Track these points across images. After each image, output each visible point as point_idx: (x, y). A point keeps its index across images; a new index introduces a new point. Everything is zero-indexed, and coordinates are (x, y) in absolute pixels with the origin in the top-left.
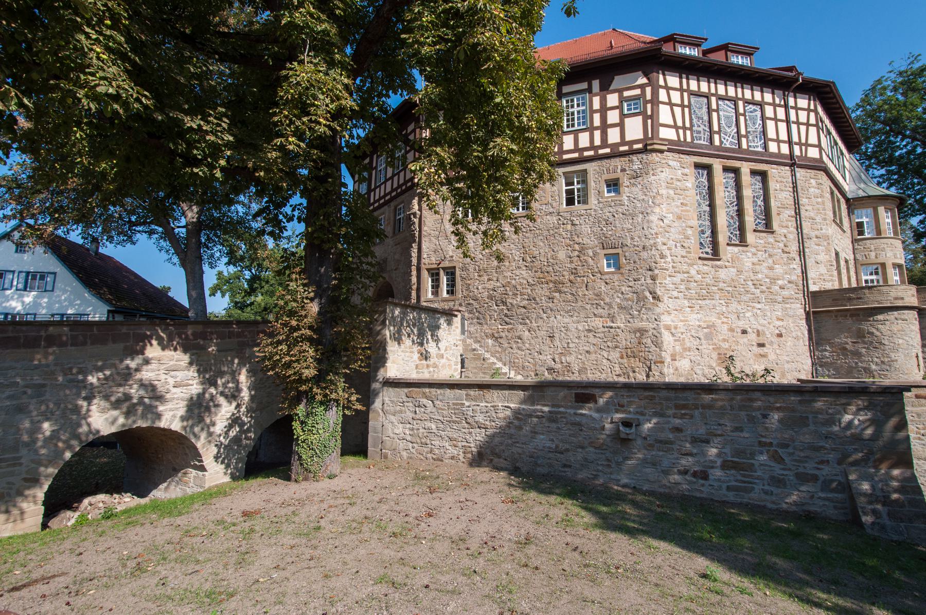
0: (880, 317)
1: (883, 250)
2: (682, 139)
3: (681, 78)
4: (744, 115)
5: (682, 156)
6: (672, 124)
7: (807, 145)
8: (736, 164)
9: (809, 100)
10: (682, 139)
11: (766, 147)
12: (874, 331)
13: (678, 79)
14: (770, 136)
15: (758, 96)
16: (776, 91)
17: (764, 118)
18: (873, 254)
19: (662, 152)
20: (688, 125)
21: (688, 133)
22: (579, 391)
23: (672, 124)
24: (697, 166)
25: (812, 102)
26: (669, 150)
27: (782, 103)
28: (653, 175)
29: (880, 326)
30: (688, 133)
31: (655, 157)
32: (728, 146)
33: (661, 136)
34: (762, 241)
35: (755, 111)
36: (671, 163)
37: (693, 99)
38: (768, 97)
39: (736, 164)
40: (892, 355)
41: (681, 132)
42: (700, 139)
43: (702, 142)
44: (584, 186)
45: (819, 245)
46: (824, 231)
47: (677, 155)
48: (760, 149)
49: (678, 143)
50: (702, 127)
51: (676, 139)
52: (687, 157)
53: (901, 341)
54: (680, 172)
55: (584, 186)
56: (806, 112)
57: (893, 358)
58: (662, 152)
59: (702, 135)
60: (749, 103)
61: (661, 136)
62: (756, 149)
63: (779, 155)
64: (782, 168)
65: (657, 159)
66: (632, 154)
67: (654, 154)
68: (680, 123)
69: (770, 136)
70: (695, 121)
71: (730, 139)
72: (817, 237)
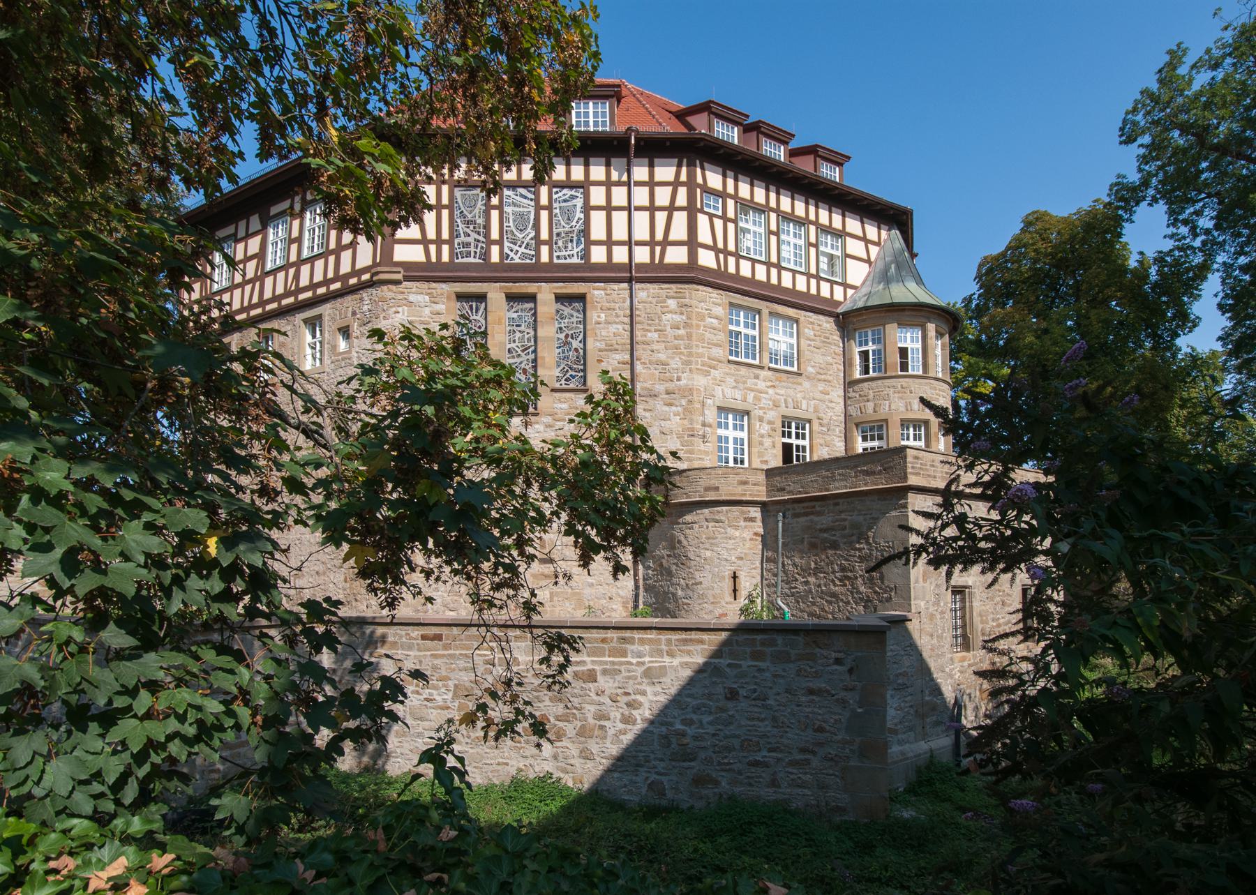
0: (688, 518)
1: (887, 398)
2: (434, 259)
3: (725, 176)
4: (549, 208)
5: (434, 285)
6: (711, 243)
7: (666, 243)
8: (530, 288)
9: (679, 166)
10: (434, 259)
11: (586, 255)
12: (682, 538)
13: (720, 177)
14: (594, 237)
15: (578, 173)
16: (613, 160)
17: (587, 208)
18: (870, 405)
19: (397, 282)
20: (445, 235)
21: (445, 248)
22: (669, 621)
23: (711, 243)
24: (460, 297)
25: (684, 169)
26: (407, 279)
27: (625, 178)
28: (385, 318)
29: (688, 531)
30: (445, 248)
31: (385, 291)
32: (517, 260)
33: (396, 258)
34: (564, 406)
35: (573, 197)
36: (412, 298)
37: (458, 193)
38: (598, 172)
39: (530, 288)
40: (697, 575)
41: (433, 248)
42: (468, 254)
43: (471, 260)
44: (881, 347)
45: (671, 405)
46: (683, 382)
47: (425, 285)
48: (575, 260)
49: (428, 265)
50: (474, 235)
51: (424, 260)
52: (443, 286)
53: (708, 554)
54: (427, 311)
55: (881, 347)
56: (646, 189)
57: (699, 580)
58: (397, 282)
59: (472, 249)
60: (563, 187)
61: (396, 258)
62: (568, 261)
63: (610, 265)
64: (615, 286)
65: (390, 295)
66: (362, 288)
67: (385, 288)
68: (720, 245)
69: (594, 237)
70: (462, 227)
71: (522, 250)
72: (668, 393)
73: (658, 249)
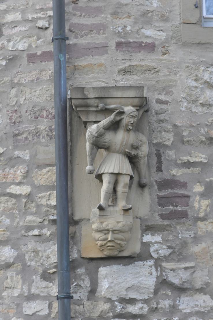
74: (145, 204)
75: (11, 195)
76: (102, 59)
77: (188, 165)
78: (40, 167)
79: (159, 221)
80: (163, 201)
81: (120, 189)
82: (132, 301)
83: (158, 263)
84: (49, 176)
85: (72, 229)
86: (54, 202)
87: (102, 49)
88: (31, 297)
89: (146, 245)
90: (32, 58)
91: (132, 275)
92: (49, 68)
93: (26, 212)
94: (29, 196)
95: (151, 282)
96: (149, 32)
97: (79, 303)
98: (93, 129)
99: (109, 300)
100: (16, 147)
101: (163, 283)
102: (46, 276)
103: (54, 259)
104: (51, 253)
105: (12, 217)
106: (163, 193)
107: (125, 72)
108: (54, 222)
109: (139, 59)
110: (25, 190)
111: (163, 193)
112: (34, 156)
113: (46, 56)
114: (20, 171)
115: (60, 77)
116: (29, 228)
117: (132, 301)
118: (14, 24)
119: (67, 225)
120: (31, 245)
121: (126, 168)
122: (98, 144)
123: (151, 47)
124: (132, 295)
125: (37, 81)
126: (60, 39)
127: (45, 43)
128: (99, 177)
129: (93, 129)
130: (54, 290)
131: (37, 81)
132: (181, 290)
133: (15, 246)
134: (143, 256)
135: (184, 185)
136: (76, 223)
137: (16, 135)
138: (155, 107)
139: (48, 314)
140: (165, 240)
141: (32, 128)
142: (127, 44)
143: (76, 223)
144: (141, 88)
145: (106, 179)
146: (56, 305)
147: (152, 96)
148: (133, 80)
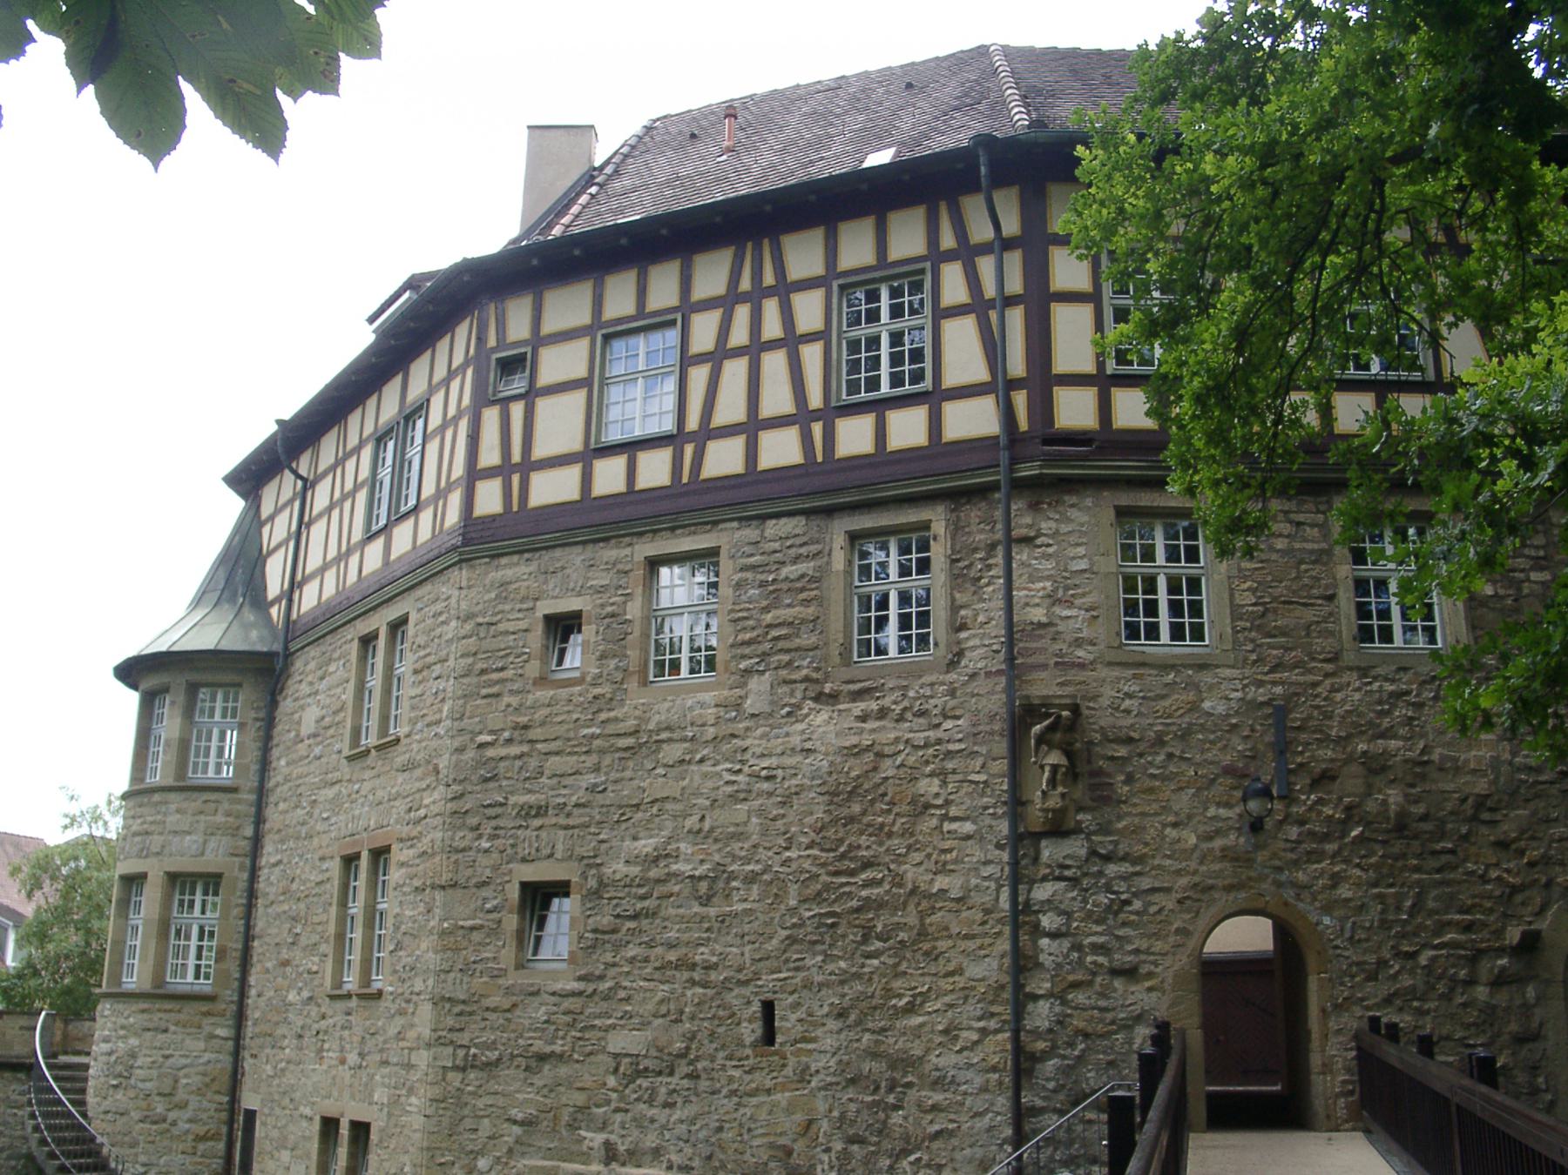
73: (817, 429)
74: (1079, 792)
75: (971, 782)
76: (1043, 675)
77: (1112, 758)
78: (994, 759)
79: (1090, 803)
80: (1093, 788)
81: (1059, 777)
82: (1068, 867)
83: (1088, 836)
84: (1001, 766)
85: (1020, 809)
86: (1005, 787)
87: (1044, 666)
88: (987, 863)
89: (1080, 822)
90: (988, 674)
91: (883, 713)
92: (1003, 681)
93: (983, 794)
94: (985, 782)
95: (1083, 852)
96: (1080, 653)
97: (1026, 867)
98: (1037, 728)
99: (1049, 866)
100: (975, 744)
101: (1093, 853)
102: (999, 846)
103: (1006, 831)
104: (1004, 827)
105: (973, 799)
106: (344, 1130)
107: (1061, 684)
108: (1005, 803)
109: (1072, 675)
110: (983, 777)
111: (344, 1130)
112: (989, 751)
113: (999, 672)
114: (979, 762)
115: (1010, 690)
116: (986, 808)
117: (1068, 867)
118: (974, 648)
119: (1016, 803)
120: (988, 821)
121: (1064, 761)
122: (1041, 740)
123: (1082, 666)
124: (1068, 862)
125: (992, 692)
126: (1011, 659)
127: (998, 664)
128: (1042, 767)
129: (1037, 728)
130: (1005, 856)
131: (992, 692)
132: (1107, 858)
133: (974, 822)
134: (1077, 831)
135: (1109, 775)
136: (1023, 804)
137: (975, 735)
138: (1086, 712)
139: (1159, 402)
140: (1094, 819)
141: (988, 728)
142: (1063, 663)
143: (1023, 804)
144: (1075, 697)
145: (1047, 769)
146: (1007, 869)
147: (1084, 705)
148: (1069, 690)
